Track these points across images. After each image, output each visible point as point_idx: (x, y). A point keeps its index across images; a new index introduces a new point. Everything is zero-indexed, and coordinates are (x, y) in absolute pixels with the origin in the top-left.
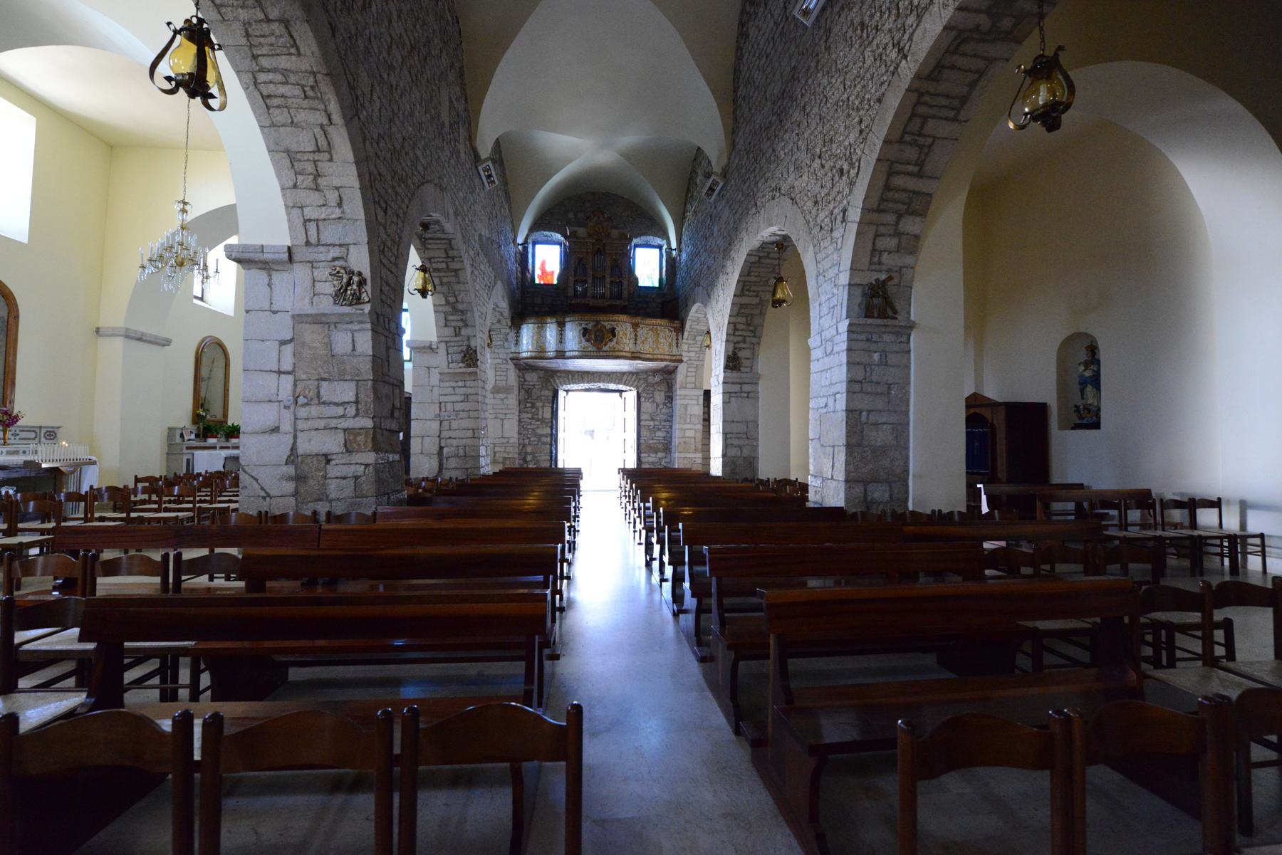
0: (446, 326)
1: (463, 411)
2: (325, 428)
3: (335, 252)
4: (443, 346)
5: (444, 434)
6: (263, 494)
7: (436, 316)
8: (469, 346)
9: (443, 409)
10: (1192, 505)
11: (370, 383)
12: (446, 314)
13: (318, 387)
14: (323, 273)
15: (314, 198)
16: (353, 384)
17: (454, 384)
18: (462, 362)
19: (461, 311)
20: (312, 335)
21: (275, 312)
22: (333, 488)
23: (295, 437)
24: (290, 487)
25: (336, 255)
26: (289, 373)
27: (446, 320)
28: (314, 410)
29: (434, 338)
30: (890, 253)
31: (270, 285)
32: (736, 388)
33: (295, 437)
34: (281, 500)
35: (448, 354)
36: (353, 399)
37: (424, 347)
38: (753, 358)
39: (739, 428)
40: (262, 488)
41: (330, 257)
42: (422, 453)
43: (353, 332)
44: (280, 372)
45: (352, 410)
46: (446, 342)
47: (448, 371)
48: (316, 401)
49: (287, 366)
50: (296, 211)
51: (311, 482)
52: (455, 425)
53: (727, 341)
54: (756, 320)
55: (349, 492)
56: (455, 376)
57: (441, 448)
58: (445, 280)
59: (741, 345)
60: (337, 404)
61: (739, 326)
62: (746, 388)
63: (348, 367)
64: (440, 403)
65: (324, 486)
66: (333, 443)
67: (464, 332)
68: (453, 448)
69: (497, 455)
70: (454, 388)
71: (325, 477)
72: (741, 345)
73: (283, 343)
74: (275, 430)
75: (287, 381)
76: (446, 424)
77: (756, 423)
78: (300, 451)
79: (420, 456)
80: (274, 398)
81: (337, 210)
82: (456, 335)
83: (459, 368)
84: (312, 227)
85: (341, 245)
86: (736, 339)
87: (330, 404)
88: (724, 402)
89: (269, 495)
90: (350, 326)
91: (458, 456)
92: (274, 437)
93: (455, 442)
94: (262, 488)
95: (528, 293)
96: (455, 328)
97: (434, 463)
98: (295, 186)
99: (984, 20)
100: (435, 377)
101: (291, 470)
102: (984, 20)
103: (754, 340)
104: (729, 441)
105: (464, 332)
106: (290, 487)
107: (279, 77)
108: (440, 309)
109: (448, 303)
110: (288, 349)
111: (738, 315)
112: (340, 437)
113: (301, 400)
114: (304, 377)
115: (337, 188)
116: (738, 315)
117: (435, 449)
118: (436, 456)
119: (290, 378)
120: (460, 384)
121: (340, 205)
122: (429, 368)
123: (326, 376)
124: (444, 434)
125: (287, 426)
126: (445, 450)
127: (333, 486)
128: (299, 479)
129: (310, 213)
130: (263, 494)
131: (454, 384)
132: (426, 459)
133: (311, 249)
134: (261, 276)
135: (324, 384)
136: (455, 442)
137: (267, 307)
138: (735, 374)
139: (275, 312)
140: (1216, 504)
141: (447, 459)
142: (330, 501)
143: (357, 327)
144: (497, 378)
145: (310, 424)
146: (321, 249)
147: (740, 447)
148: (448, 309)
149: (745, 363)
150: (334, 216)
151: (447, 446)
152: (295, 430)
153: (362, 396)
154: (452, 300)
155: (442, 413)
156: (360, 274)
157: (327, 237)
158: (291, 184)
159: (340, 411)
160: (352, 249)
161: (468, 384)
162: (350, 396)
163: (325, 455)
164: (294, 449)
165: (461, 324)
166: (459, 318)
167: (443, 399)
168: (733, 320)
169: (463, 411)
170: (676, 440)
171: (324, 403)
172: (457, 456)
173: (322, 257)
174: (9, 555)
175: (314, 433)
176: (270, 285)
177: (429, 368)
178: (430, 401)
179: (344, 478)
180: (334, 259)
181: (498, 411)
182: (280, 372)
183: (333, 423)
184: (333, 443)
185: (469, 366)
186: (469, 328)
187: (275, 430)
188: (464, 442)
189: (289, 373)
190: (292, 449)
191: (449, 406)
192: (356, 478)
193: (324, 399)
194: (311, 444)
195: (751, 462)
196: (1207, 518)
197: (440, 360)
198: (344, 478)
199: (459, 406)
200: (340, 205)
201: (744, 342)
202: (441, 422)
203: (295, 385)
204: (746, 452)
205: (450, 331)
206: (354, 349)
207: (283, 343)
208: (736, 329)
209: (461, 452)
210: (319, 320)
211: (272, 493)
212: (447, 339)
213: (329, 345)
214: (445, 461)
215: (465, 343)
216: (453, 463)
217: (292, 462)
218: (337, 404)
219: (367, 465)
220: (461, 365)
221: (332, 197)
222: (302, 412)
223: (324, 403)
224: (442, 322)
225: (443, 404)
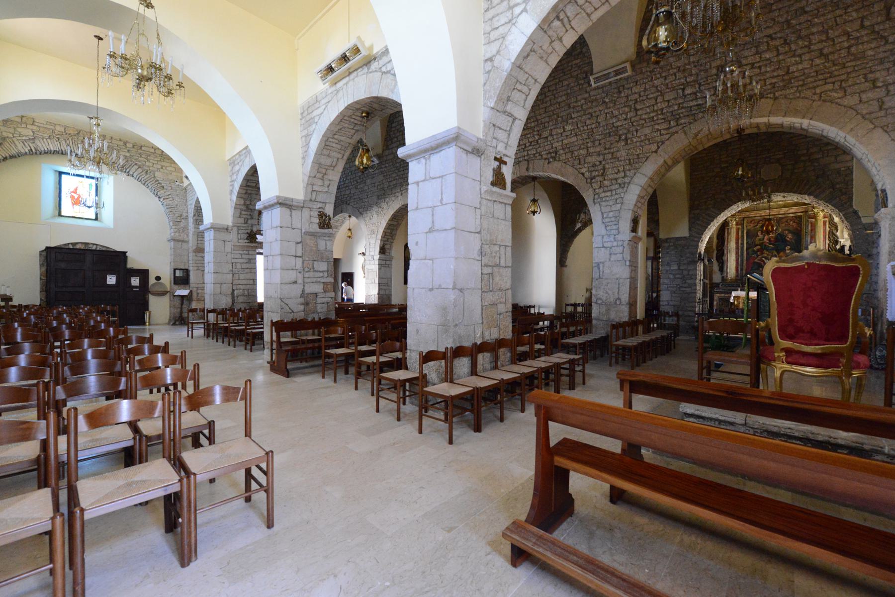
0: (240, 217)
1: (247, 268)
2: (316, 282)
3: (320, 205)
4: (235, 229)
5: (235, 282)
6: (290, 311)
7: (235, 211)
8: (252, 230)
9: (234, 267)
10: (530, 307)
11: (332, 263)
12: (241, 210)
13: (313, 264)
14: (315, 214)
15: (320, 182)
16: (326, 263)
17: (241, 252)
18: (247, 239)
19: (251, 210)
20: (310, 241)
21: (293, 229)
22: (319, 308)
23: (304, 286)
24: (302, 307)
25: (321, 206)
26: (300, 257)
27: (241, 214)
28: (311, 274)
29: (230, 224)
30: (668, 313)
31: (291, 216)
32: (383, 262)
33: (304, 286)
34: (298, 314)
35: (238, 234)
36: (326, 270)
37: (223, 228)
38: (390, 249)
39: (384, 281)
40: (290, 308)
41: (318, 207)
42: (221, 293)
43: (326, 240)
44: (296, 256)
45: (326, 274)
46: (238, 227)
47: (238, 244)
48: (312, 270)
49: (299, 254)
50: (310, 187)
51: (311, 306)
52: (242, 276)
53: (381, 240)
54: (394, 232)
55: (325, 309)
56: (243, 248)
57: (233, 290)
58: (249, 192)
59: (386, 243)
60: (320, 272)
61: (387, 234)
62: (388, 262)
63: (324, 256)
64: (232, 263)
65: (315, 307)
66: (318, 288)
67: (250, 222)
68: (241, 291)
69: (200, 295)
70: (241, 254)
71: (316, 303)
72: (386, 243)
73: (297, 243)
74: (295, 282)
75: (300, 261)
76: (236, 276)
77: (391, 278)
78: (306, 292)
79: (220, 295)
80: (294, 268)
81: (327, 188)
82: (245, 223)
83: (244, 242)
84: (314, 194)
85: (323, 203)
86: (384, 239)
87: (317, 271)
88: (379, 269)
89: (293, 312)
90: (325, 238)
91: (244, 296)
92: (295, 286)
93: (242, 287)
94: (290, 308)
95: (20, 135)
96: (245, 219)
97: (229, 300)
98: (315, 177)
99: (520, 180)
100: (229, 248)
101: (302, 300)
102: (520, 180)
103: (392, 241)
104: (381, 287)
105: (250, 222)
106: (302, 307)
107: (337, 142)
108: (238, 207)
109: (245, 204)
110: (300, 246)
111: (388, 229)
112: (321, 286)
113: (307, 269)
114: (307, 259)
115: (330, 180)
116: (388, 229)
117: (230, 291)
118: (230, 295)
119: (301, 259)
120: (245, 252)
121: (328, 187)
122: (224, 241)
123: (316, 259)
124: (235, 282)
125: (300, 281)
126: (236, 292)
127: (319, 306)
128: (307, 304)
129: (316, 188)
130: (290, 311)
131: (241, 252)
132: (224, 297)
133: (312, 203)
134: (287, 211)
135: (315, 262)
136: (242, 287)
137: (290, 226)
138: (383, 256)
139: (293, 229)
140: (534, 307)
141: (237, 297)
142: (318, 313)
143: (328, 238)
144: (199, 242)
145: (309, 280)
146: (315, 203)
147: (385, 290)
148: (243, 208)
149: (388, 251)
150: (324, 191)
151: (237, 289)
152: (304, 282)
153: (330, 269)
154: (248, 203)
155: (234, 270)
156: (329, 216)
157: (319, 199)
158: (313, 176)
159: (321, 274)
160: (327, 205)
161: (250, 253)
162: (325, 268)
163: (316, 294)
164: (303, 291)
165: (249, 217)
166: (249, 213)
167: (234, 261)
168: (386, 230)
169: (247, 268)
170: (206, 281)
171: (315, 271)
172: (243, 295)
173: (315, 207)
174: (776, 272)
175: (312, 284)
176: (291, 216)
177: (224, 241)
178: (226, 262)
179: (323, 303)
180: (320, 208)
181: (199, 265)
182: (296, 256)
183: (319, 280)
184: (318, 288)
185: (251, 242)
186: (253, 220)
187: (295, 282)
188: (248, 287)
189: (300, 257)
190: (303, 291)
191: (239, 266)
192: (328, 303)
193: (316, 269)
194: (312, 288)
195: (389, 297)
196: (532, 311)
197: (233, 237)
198: (323, 303)
199: (244, 266)
200: (328, 187)
201: (388, 241)
202: (233, 275)
203: (303, 263)
204: (387, 292)
205: (242, 220)
206: (326, 248)
207: (297, 243)
208: (385, 235)
209: (246, 293)
210: (313, 234)
211: (295, 311)
212: (239, 225)
213: (316, 245)
214: (236, 298)
215: (249, 228)
216: (241, 299)
217: (303, 297)
218: (320, 272)
219: (332, 298)
220: (246, 241)
221: (327, 183)
222: (307, 275)
223: (315, 271)
224: (238, 215)
225: (234, 264)
